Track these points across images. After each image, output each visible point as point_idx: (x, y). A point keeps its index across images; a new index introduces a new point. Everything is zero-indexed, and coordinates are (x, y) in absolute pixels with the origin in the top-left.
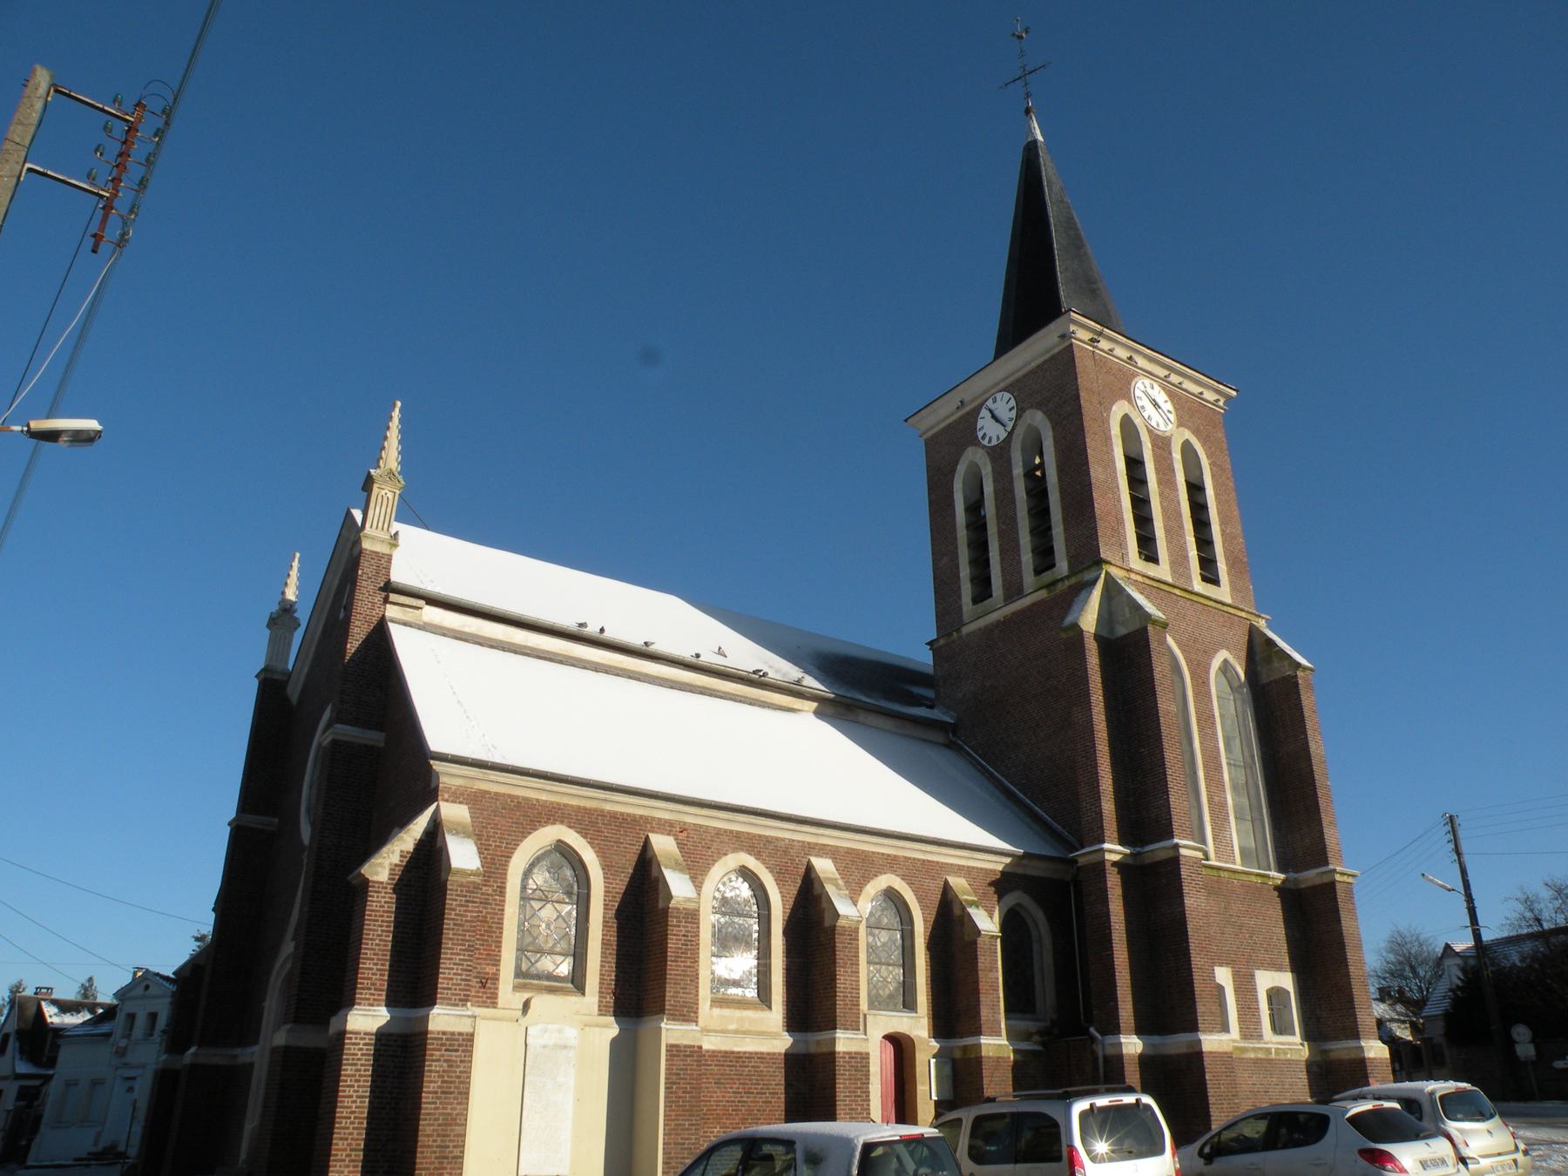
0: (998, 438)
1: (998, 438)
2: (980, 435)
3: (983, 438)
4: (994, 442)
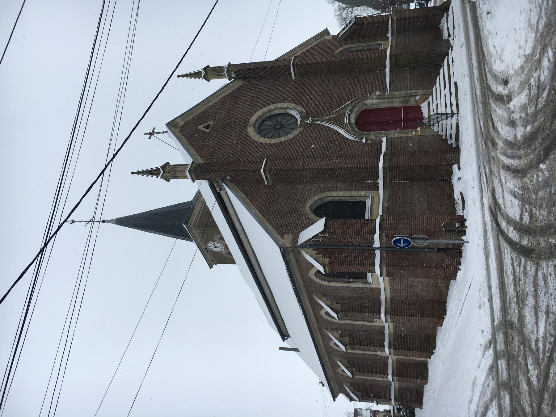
2: (220, 251)
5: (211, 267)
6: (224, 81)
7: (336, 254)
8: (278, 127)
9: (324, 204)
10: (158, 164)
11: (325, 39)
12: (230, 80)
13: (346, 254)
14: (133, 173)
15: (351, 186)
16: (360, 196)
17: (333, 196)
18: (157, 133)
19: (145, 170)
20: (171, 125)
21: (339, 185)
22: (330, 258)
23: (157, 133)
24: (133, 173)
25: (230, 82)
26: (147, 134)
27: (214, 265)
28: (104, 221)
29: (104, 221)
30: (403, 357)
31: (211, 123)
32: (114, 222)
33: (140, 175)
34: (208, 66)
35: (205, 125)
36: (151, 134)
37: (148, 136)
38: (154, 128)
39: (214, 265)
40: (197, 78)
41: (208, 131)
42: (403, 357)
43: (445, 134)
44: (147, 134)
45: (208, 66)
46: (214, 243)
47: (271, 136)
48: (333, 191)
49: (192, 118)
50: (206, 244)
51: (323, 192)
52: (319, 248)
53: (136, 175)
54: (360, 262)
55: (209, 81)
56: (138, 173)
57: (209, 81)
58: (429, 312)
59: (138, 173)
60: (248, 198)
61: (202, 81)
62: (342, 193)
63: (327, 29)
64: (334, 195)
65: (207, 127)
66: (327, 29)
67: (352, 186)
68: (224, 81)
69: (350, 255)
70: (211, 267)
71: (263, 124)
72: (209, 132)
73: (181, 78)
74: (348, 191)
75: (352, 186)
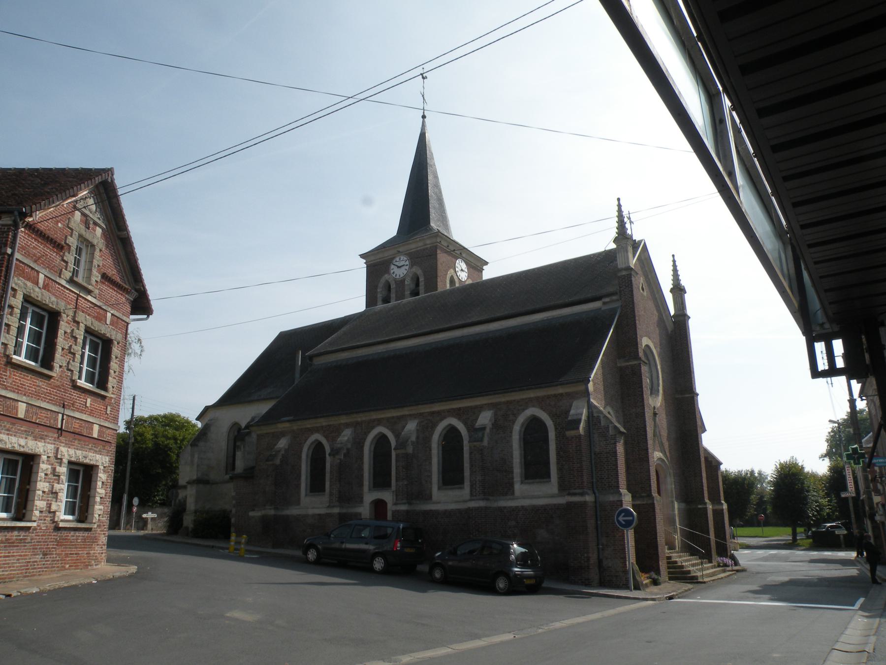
0: (400, 276)
1: (400, 276)
2: (392, 271)
3: (394, 273)
4: (398, 277)
5: (363, 256)
10: (684, 282)
27: (365, 261)
28: (424, 117)
29: (424, 117)
30: (674, 570)
32: (423, 132)
39: (365, 261)
40: (617, 231)
42: (674, 570)
43: (838, 566)
46: (407, 265)
47: (399, 266)
50: (405, 254)
53: (672, 259)
56: (674, 261)
58: (100, 531)
59: (674, 261)
70: (363, 256)
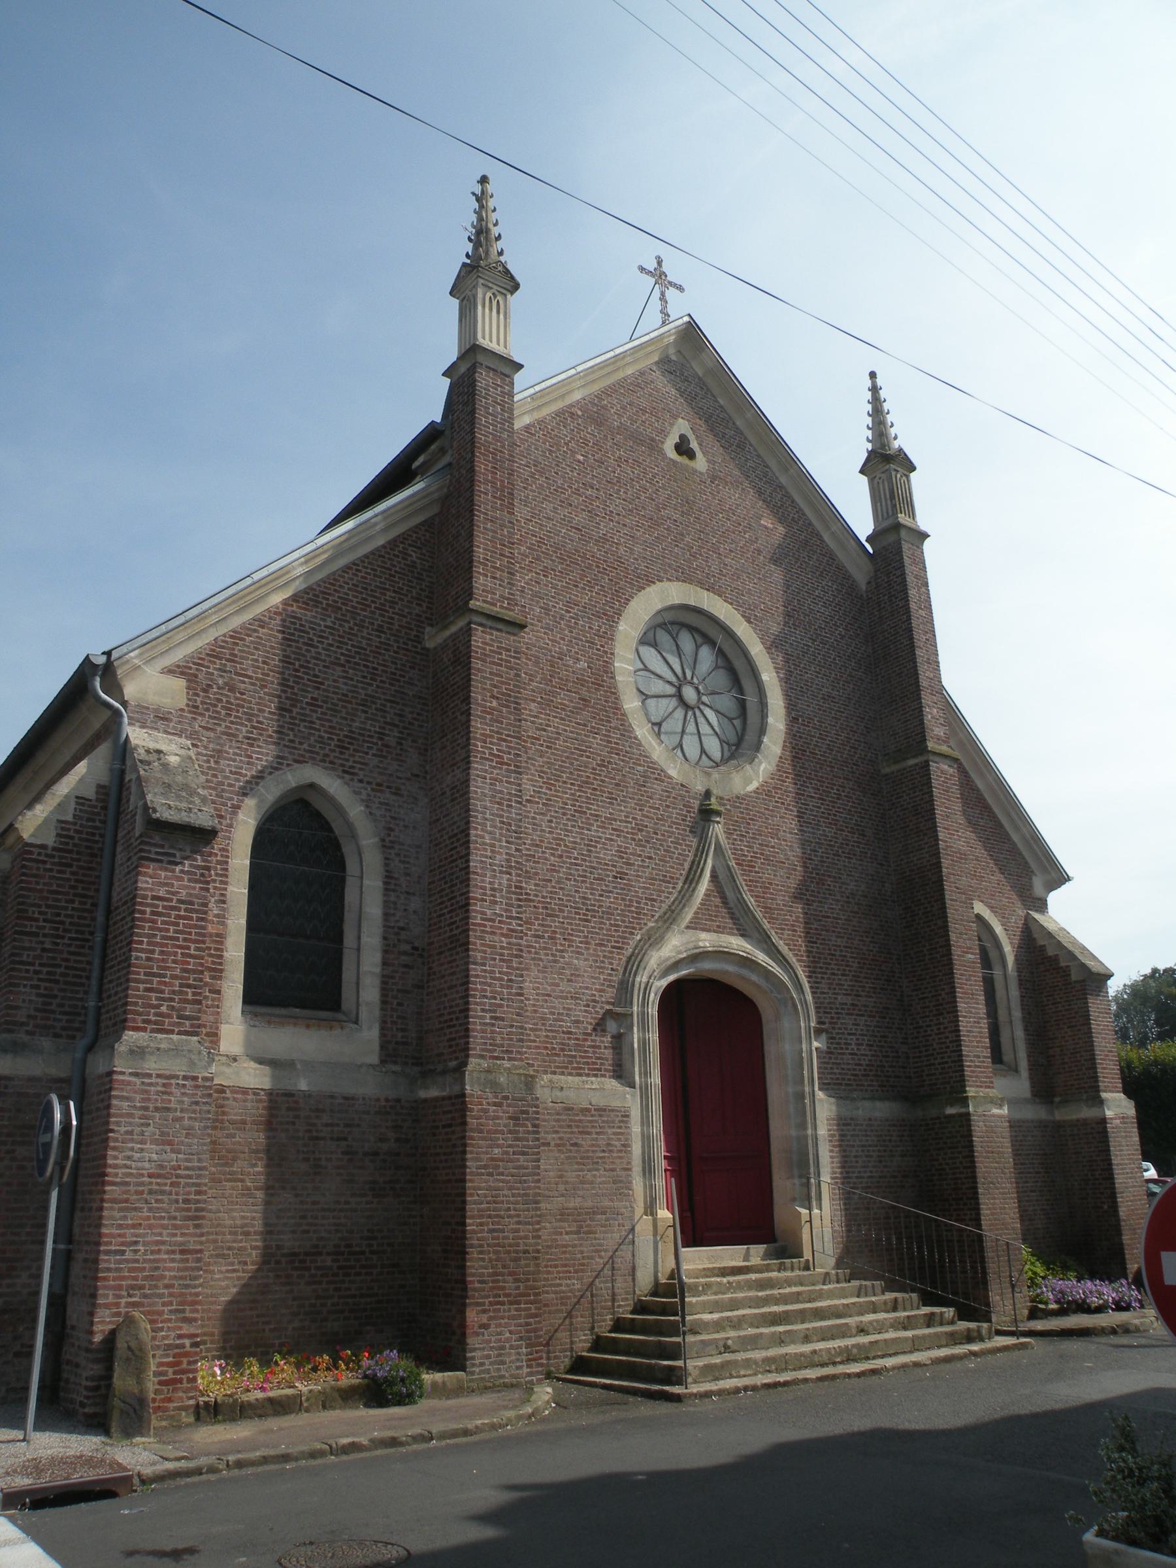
6: (862, 522)
7: (73, 873)
8: (689, 693)
9: (337, 846)
11: (1032, 872)
12: (868, 539)
13: (71, 916)
14: (873, 375)
15: (407, 947)
16: (358, 984)
17: (362, 878)
18: (663, 294)
19: (886, 406)
20: (691, 335)
21: (415, 903)
22: (54, 849)
23: (663, 294)
24: (873, 375)
25: (863, 539)
26: (660, 263)
31: (701, 463)
33: (869, 395)
34: (912, 468)
35: (694, 445)
36: (659, 275)
37: (651, 265)
38: (680, 288)
40: (869, 434)
41: (672, 454)
44: (660, 263)
45: (912, 468)
48: (387, 877)
49: (721, 407)
51: (383, 840)
52: (105, 808)
54: (27, 971)
55: (862, 471)
56: (875, 389)
57: (862, 471)
60: (366, 556)
61: (860, 449)
62: (374, 909)
63: (1069, 879)
64: (366, 882)
65: (683, 448)
66: (1069, 879)
67: (405, 953)
68: (862, 522)
69: (65, 930)
71: (699, 640)
72: (661, 452)
73: (869, 384)
74: (385, 938)
75: (405, 953)
